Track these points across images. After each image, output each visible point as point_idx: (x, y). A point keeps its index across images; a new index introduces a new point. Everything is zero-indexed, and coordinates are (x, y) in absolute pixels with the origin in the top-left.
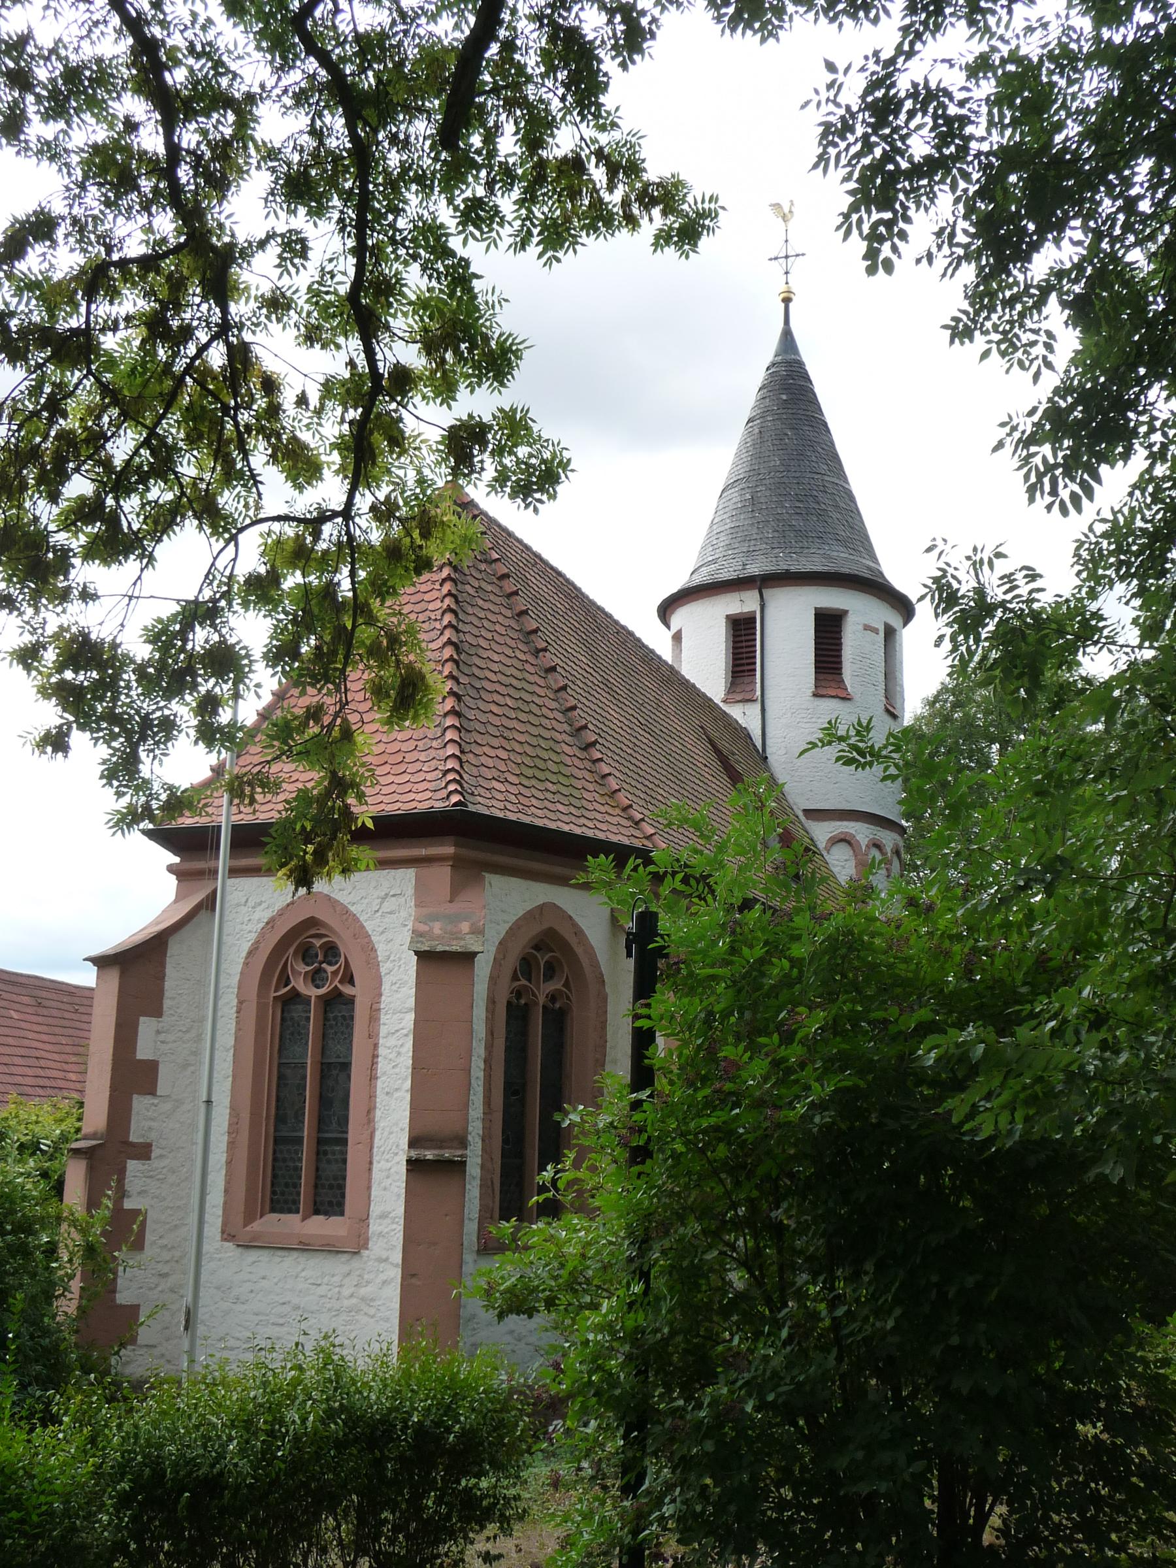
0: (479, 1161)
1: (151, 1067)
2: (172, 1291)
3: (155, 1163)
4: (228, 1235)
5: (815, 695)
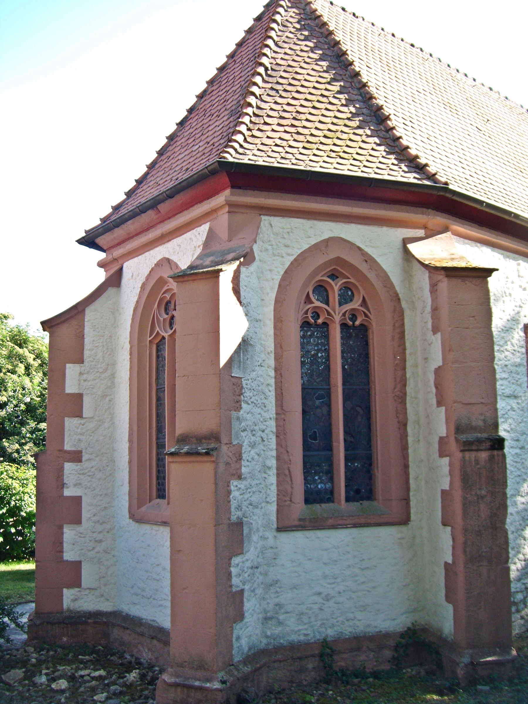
0: (274, 453)
1: (78, 399)
2: (105, 551)
3: (85, 464)
4: (132, 516)
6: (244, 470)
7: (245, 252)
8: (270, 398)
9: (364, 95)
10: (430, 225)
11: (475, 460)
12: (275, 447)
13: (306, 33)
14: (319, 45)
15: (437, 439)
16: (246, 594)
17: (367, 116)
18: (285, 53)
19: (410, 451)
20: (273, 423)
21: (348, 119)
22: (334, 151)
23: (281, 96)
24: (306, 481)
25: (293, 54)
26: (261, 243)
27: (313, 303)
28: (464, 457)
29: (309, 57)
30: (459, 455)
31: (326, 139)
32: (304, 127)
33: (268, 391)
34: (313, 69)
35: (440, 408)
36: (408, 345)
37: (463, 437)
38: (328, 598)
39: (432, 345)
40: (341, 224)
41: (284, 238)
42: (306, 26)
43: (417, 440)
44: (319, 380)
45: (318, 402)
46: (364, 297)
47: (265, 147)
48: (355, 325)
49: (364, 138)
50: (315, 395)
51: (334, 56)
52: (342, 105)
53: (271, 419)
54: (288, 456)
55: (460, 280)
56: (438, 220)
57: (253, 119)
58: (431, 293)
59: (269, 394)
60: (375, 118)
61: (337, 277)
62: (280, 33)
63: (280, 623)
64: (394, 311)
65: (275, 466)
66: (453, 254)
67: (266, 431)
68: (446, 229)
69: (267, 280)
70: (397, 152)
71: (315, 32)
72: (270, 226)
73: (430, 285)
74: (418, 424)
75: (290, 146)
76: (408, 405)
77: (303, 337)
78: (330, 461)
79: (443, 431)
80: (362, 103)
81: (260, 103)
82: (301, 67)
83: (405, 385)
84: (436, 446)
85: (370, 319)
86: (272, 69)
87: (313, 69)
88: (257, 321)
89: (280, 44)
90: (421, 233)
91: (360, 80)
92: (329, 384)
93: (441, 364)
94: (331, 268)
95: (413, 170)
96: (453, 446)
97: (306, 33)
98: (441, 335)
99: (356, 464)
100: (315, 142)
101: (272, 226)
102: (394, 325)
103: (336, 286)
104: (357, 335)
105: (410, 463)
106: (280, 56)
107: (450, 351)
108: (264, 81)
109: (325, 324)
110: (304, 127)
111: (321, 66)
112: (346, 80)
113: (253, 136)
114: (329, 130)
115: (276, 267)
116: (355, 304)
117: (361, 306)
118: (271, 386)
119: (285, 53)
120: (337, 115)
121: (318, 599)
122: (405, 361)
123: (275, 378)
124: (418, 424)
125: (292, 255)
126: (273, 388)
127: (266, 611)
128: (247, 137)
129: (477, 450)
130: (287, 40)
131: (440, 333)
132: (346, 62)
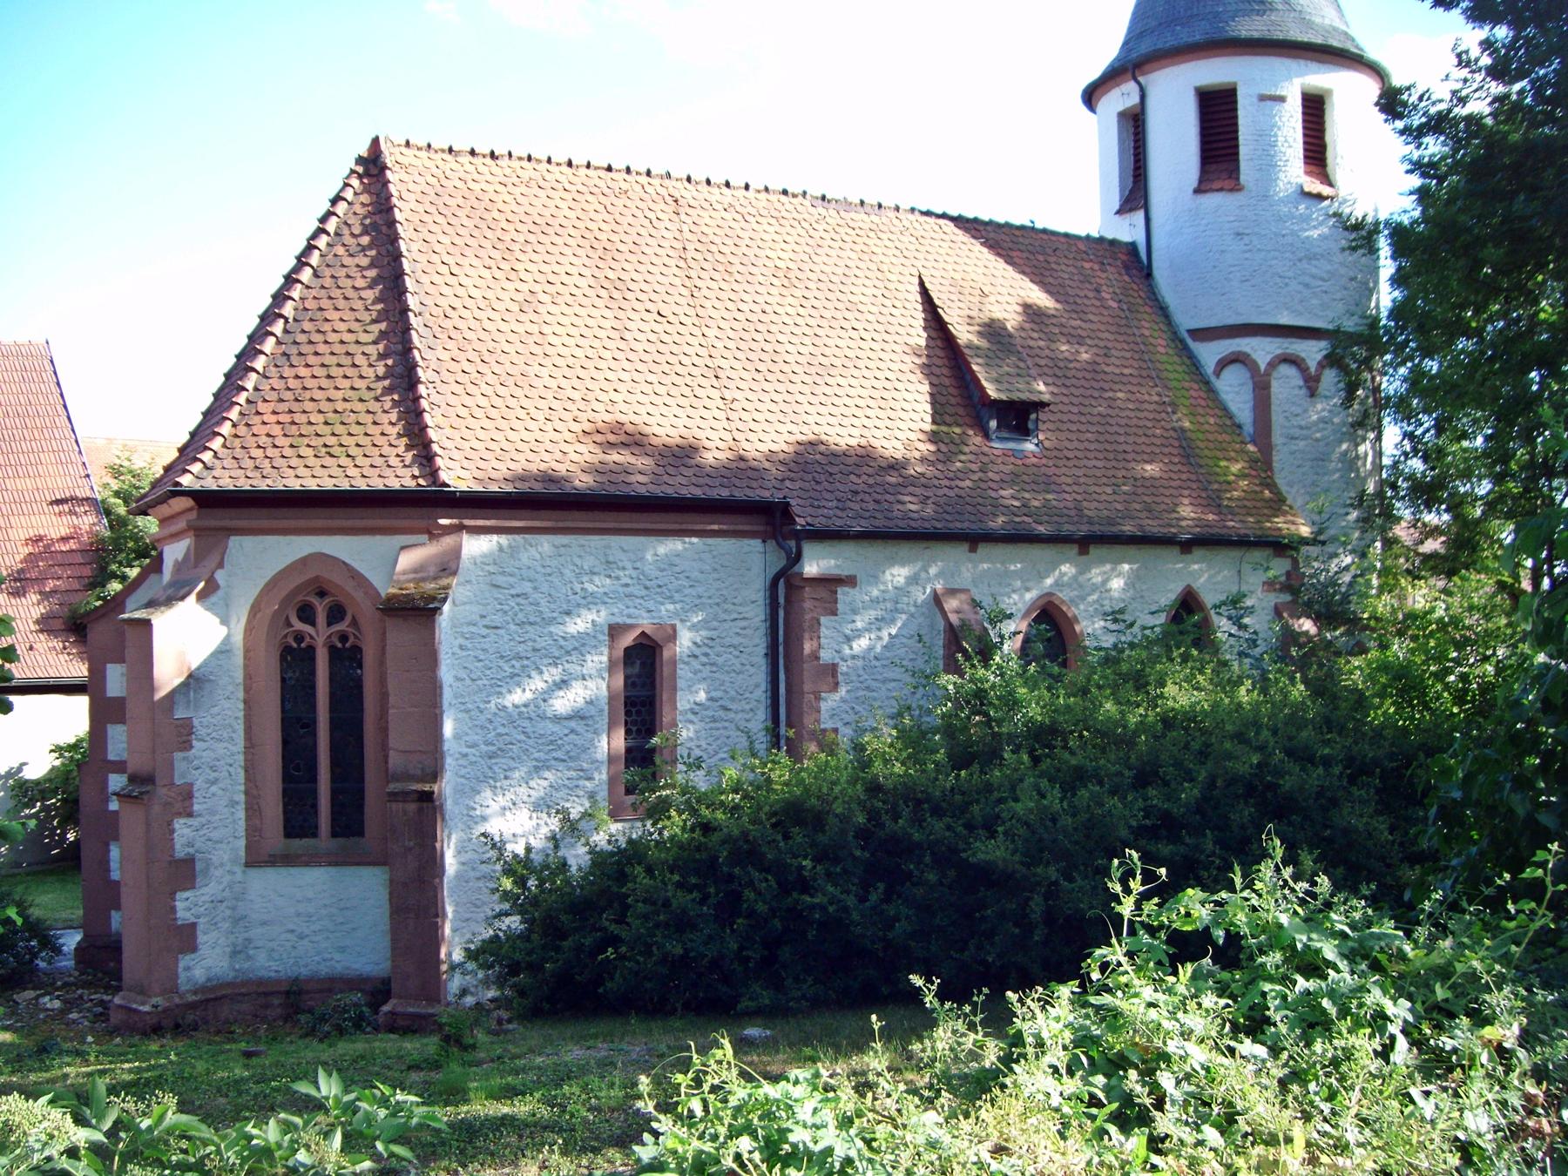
0: (242, 788)
5: (1197, 191)
6: (196, 807)
16: (200, 928)
20: (242, 757)
38: (301, 937)
50: (296, 727)
63: (249, 958)
121: (289, 936)
126: (241, 721)
127: (235, 945)
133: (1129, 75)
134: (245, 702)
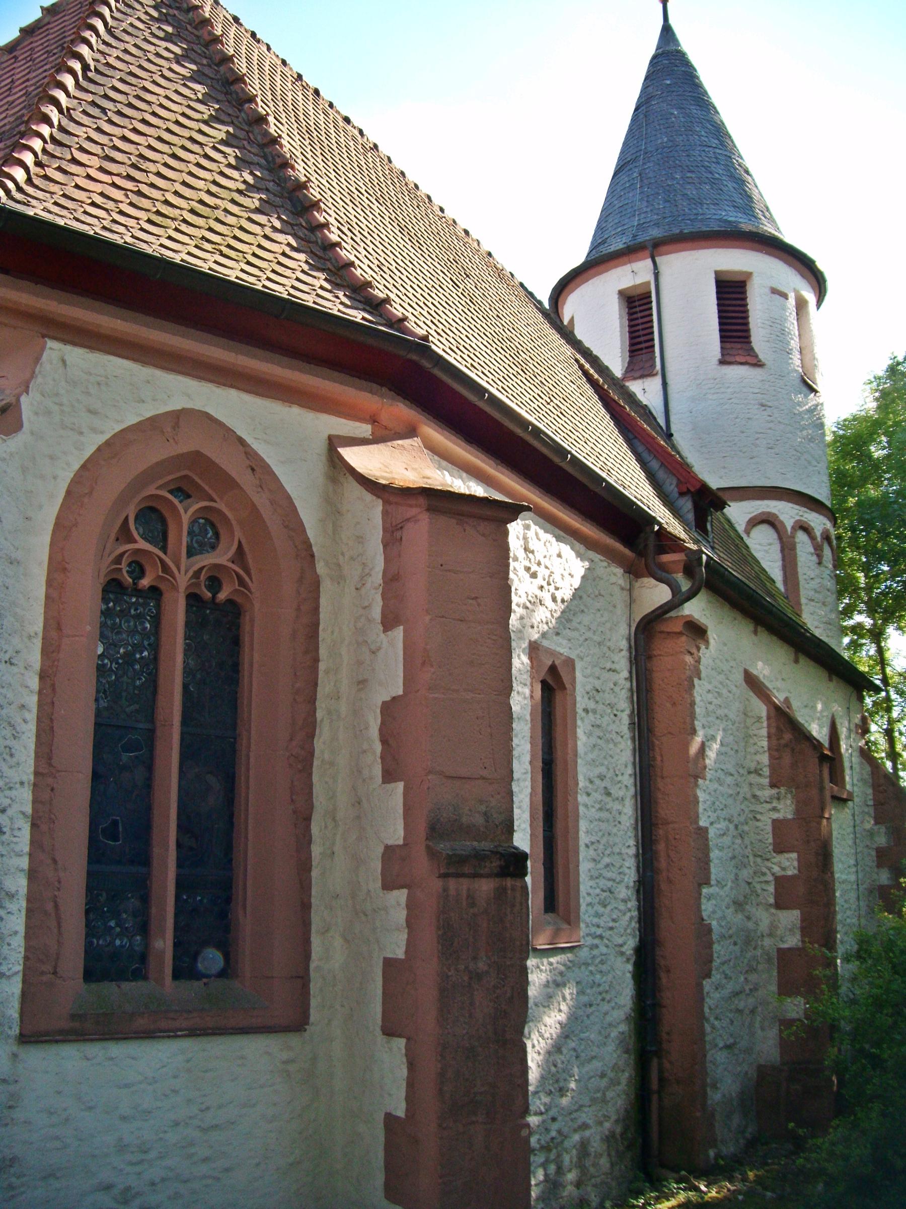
0: (24, 863)
5: (722, 362)
7: (4, 402)
8: (24, 737)
9: (270, 159)
10: (385, 418)
11: (468, 897)
12: (27, 849)
13: (170, 29)
14: (192, 55)
15: (380, 850)
17: (275, 195)
18: (126, 51)
19: (314, 873)
21: (239, 192)
22: (208, 241)
23: (110, 122)
24: (91, 931)
25: (141, 56)
26: (38, 397)
27: (136, 542)
28: (445, 890)
29: (170, 69)
30: (437, 884)
31: (195, 217)
32: (152, 185)
33: (20, 720)
34: (176, 92)
35: (393, 785)
36: (323, 652)
37: (444, 847)
39: (380, 654)
40: (210, 385)
41: (88, 393)
42: (169, 18)
43: (329, 852)
44: (133, 708)
45: (125, 757)
46: (240, 542)
47: (70, 202)
48: (217, 601)
49: (268, 231)
50: (120, 737)
51: (218, 80)
52: (229, 166)
53: (22, 783)
54: (56, 870)
55: (454, 521)
56: (401, 411)
57: (50, 147)
58: (386, 545)
59: (24, 727)
60: (292, 203)
61: (188, 496)
62: (117, 15)
64: (301, 580)
65: (23, 891)
66: (428, 478)
67: (10, 812)
68: (411, 432)
69: (42, 477)
70: (329, 269)
71: (186, 32)
72: (61, 364)
73: (385, 530)
74: (334, 819)
75: (121, 213)
76: (315, 778)
77: (106, 613)
78: (143, 888)
79: (396, 834)
80: (266, 172)
81: (65, 122)
82: (154, 82)
83: (312, 736)
84: (377, 865)
85: (249, 590)
86: (96, 69)
87: (176, 92)
88: (11, 563)
89: (117, 33)
90: (364, 430)
91: (266, 130)
92: (151, 719)
93: (401, 692)
94: (178, 475)
95: (361, 306)
96: (422, 865)
97: (170, 29)
98: (405, 631)
99: (199, 898)
100: (172, 216)
101: (65, 364)
102: (298, 609)
103: (186, 513)
104: (219, 623)
105: (313, 900)
106: (115, 53)
107: (424, 663)
108: (77, 85)
109: (155, 592)
110: (152, 185)
111: (194, 90)
112: (239, 124)
113: (46, 177)
114: (201, 202)
115: (65, 453)
116: (221, 557)
117: (233, 562)
118: (29, 711)
119: (126, 51)
120: (217, 180)
122: (316, 684)
123: (40, 692)
124: (334, 819)
125: (102, 432)
128: (33, 176)
129: (475, 876)
130: (130, 29)
131: (401, 627)
132: (241, 95)
133: (647, 253)
134: (43, 675)
